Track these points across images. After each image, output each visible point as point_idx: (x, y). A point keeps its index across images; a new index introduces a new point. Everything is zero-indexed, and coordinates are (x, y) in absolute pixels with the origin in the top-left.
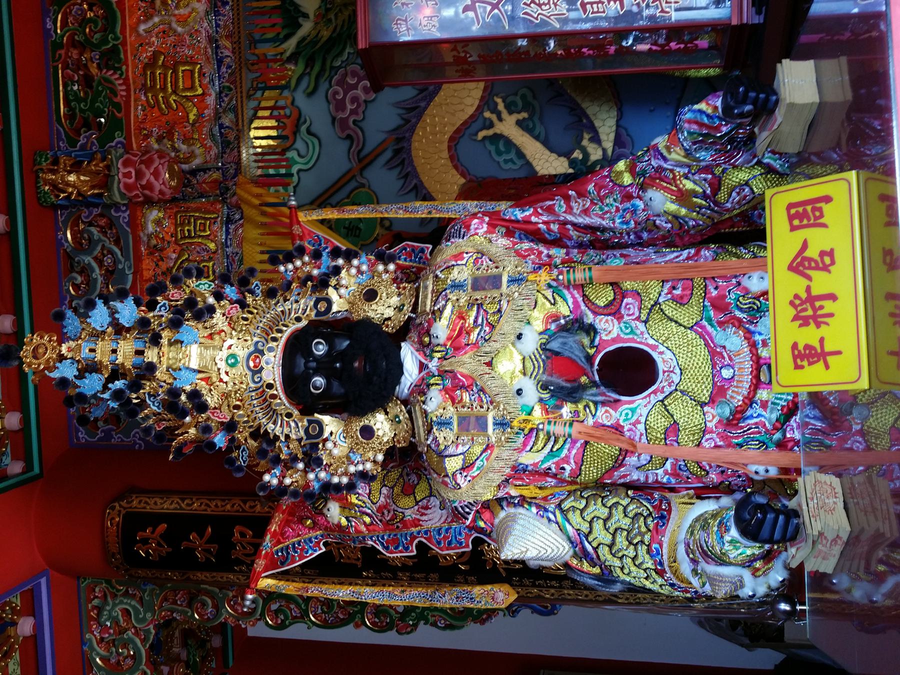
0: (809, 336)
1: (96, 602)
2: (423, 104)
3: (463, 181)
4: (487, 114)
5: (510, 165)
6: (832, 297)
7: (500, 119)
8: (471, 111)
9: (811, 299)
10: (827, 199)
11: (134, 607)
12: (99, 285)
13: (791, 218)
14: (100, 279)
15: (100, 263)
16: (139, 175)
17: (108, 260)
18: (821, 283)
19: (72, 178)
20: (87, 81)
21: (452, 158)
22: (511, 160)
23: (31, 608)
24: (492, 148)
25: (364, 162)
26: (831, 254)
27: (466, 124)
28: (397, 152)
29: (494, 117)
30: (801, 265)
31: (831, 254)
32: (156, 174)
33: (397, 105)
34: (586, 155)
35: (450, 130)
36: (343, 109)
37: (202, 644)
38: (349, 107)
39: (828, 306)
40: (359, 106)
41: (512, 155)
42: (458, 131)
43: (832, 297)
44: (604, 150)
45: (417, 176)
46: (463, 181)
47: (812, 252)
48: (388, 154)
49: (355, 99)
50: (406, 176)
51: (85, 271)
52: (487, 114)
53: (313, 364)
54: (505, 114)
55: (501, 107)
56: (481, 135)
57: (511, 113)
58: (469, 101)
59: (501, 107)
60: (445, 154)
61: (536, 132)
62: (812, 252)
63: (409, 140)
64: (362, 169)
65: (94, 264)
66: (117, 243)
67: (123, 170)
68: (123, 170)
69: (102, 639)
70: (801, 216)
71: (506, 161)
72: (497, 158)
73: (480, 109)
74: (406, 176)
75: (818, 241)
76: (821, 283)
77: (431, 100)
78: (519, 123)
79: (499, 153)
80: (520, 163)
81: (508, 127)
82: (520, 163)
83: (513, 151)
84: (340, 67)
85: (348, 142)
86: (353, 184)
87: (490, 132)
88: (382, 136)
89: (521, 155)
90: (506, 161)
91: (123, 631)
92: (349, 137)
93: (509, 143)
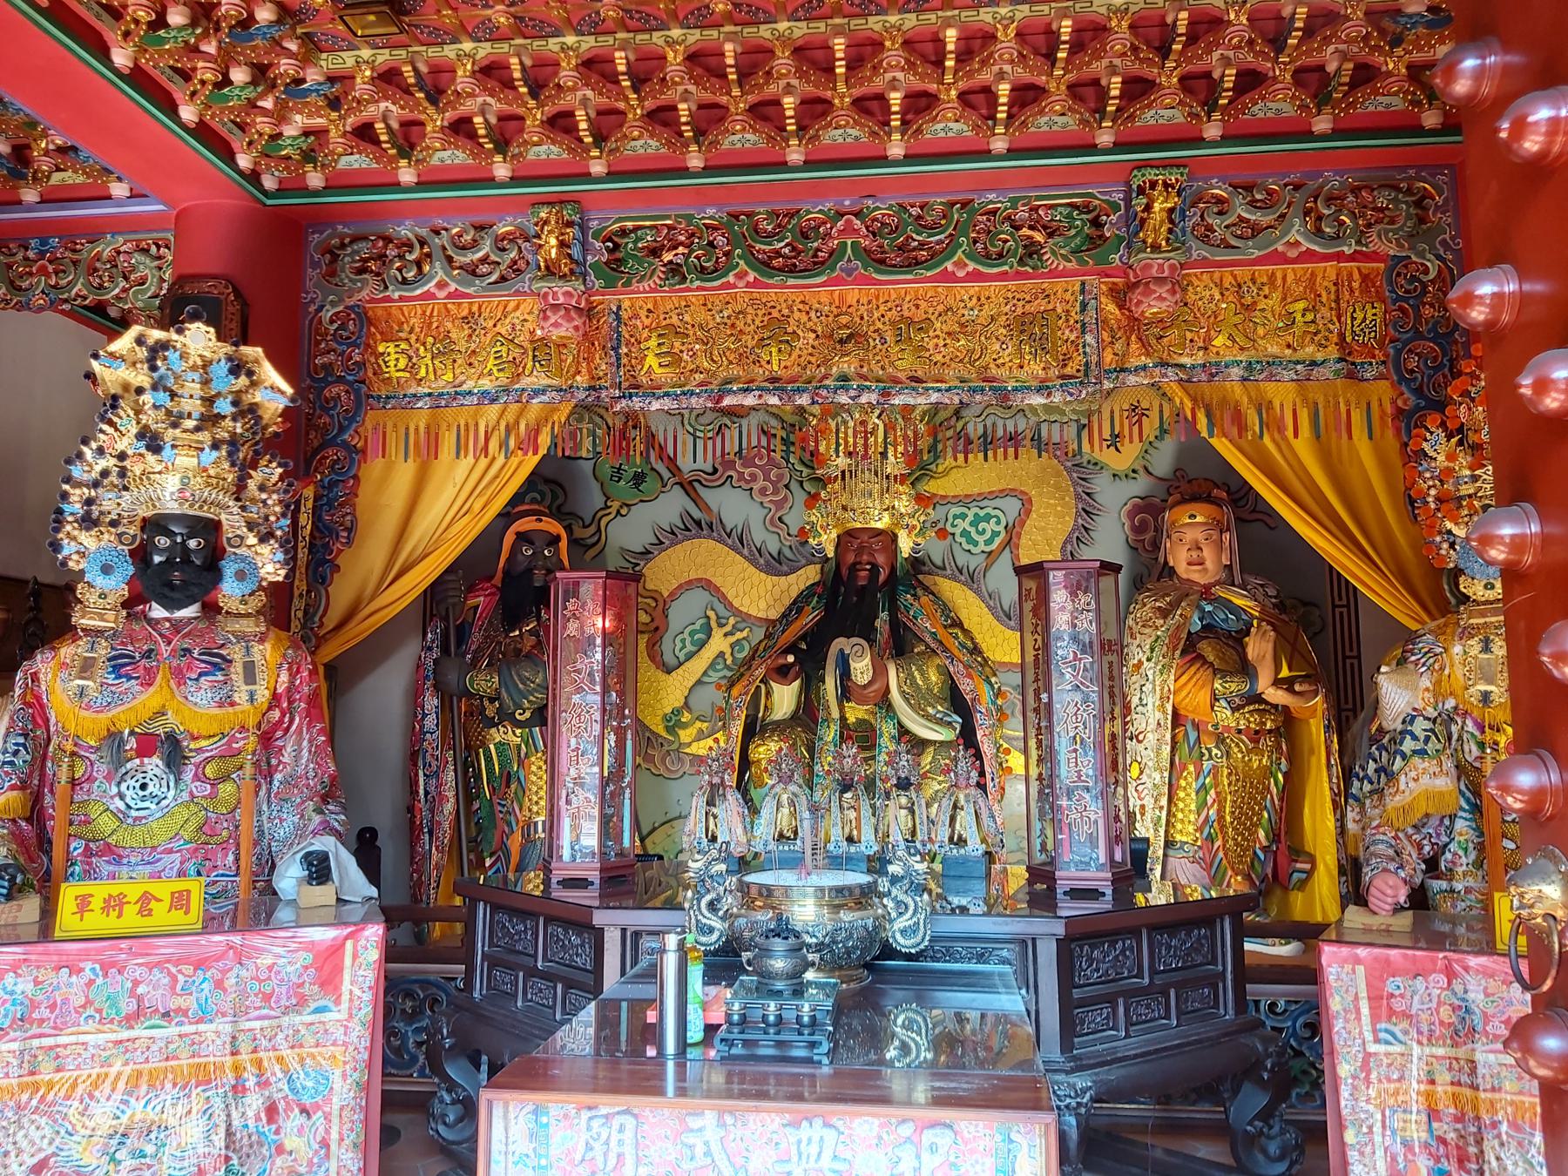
0: (97, 903)
1: (154, 249)
2: (746, 552)
3: (666, 594)
4: (732, 621)
5: (679, 645)
6: (120, 916)
7: (726, 635)
8: (736, 603)
9: (121, 905)
10: (187, 913)
11: (148, 289)
12: (463, 259)
13: (180, 892)
14: (467, 260)
15: (484, 260)
16: (555, 307)
17: (484, 269)
18: (131, 911)
19: (553, 241)
20: (655, 252)
21: (690, 582)
22: (684, 647)
23: (134, 195)
24: (697, 626)
25: (688, 487)
26: (150, 914)
27: (723, 599)
28: (698, 523)
29: (728, 628)
30: (146, 898)
31: (150, 914)
32: (556, 325)
33: (746, 525)
34: (685, 726)
35: (718, 581)
36: (745, 465)
37: (308, 156)
38: (747, 471)
39: (114, 914)
40: (747, 482)
41: (690, 648)
42: (717, 589)
43: (120, 916)
44: (689, 744)
45: (673, 544)
46: (666, 594)
47: (153, 904)
48: (696, 514)
49: (754, 477)
50: (673, 533)
51: (474, 244)
52: (732, 621)
53: (179, 540)
54: (732, 639)
55: (739, 635)
56: (711, 614)
57: (732, 646)
58: (746, 601)
59: (739, 635)
60: (693, 576)
61: (711, 673)
62: (153, 904)
63: (709, 537)
64: (681, 484)
65: (480, 254)
66: (503, 279)
67: (561, 292)
68: (561, 292)
69: (119, 253)
70: (180, 899)
71: (683, 641)
72: (687, 631)
73: (737, 613)
74: (673, 533)
75: (159, 909)
76: (131, 911)
77: (749, 561)
78: (721, 654)
79: (692, 634)
80: (682, 657)
81: (719, 643)
82: (682, 657)
83: (694, 649)
84: (788, 461)
85: (710, 470)
86: (666, 474)
87: (713, 624)
88: (715, 508)
89: (690, 657)
90: (683, 641)
91: (126, 278)
92: (715, 471)
93: (702, 645)
